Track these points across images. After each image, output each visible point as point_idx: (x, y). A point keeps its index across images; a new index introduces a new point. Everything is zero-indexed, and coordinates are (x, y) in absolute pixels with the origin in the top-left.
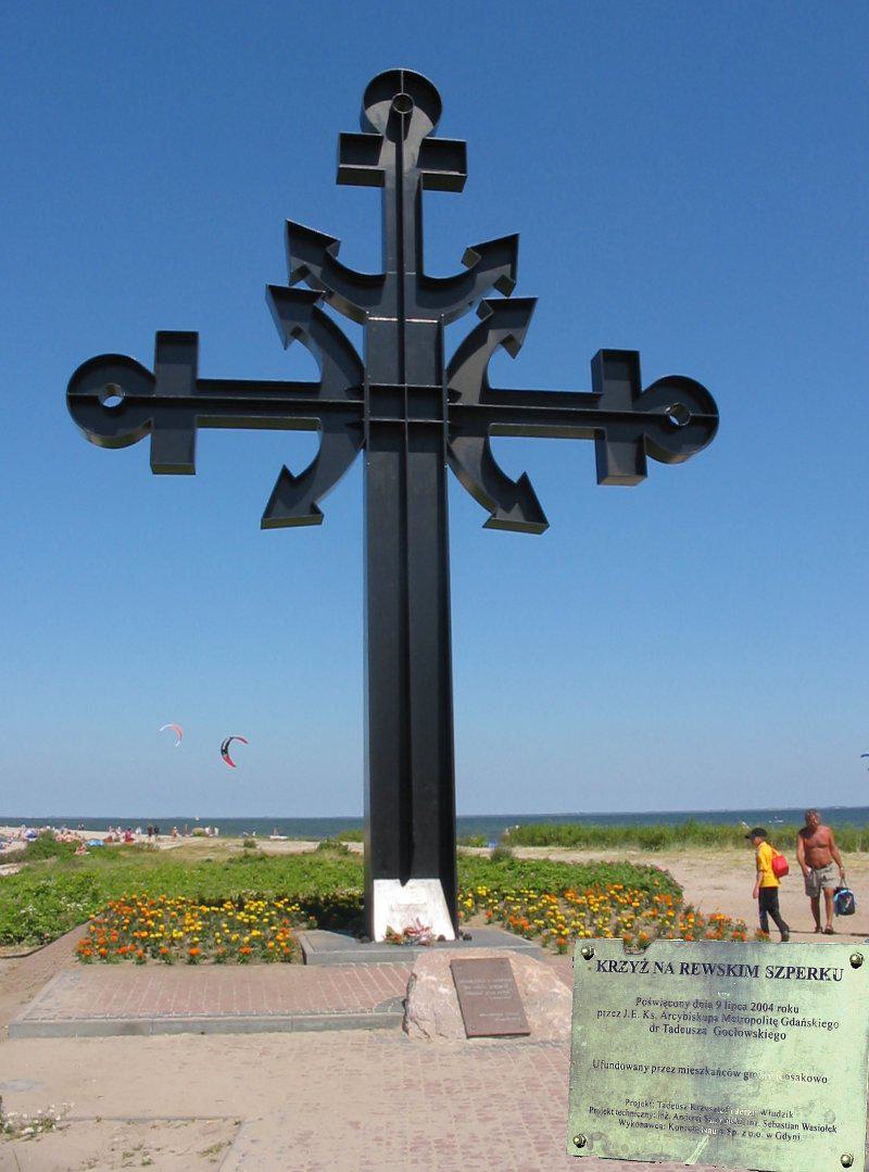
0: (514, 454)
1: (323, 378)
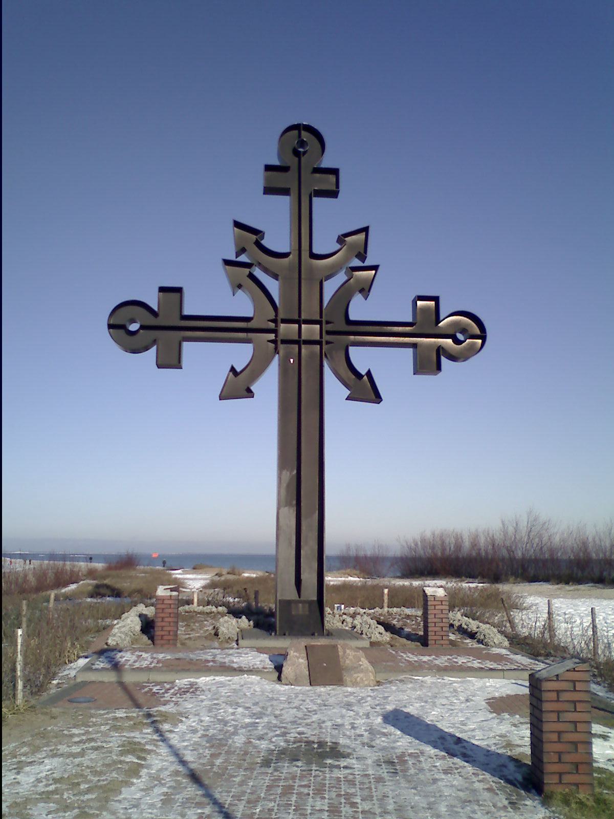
0: (362, 358)
1: (254, 315)
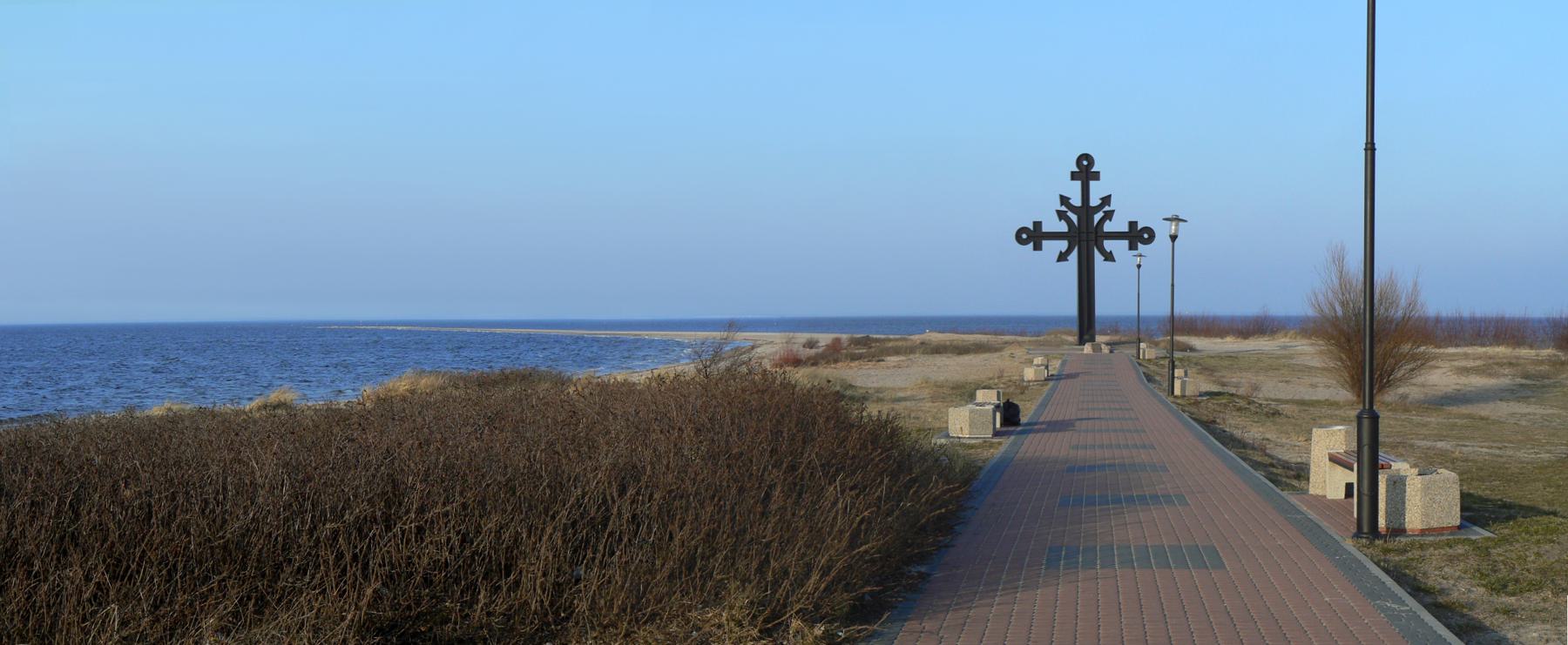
0: (1109, 245)
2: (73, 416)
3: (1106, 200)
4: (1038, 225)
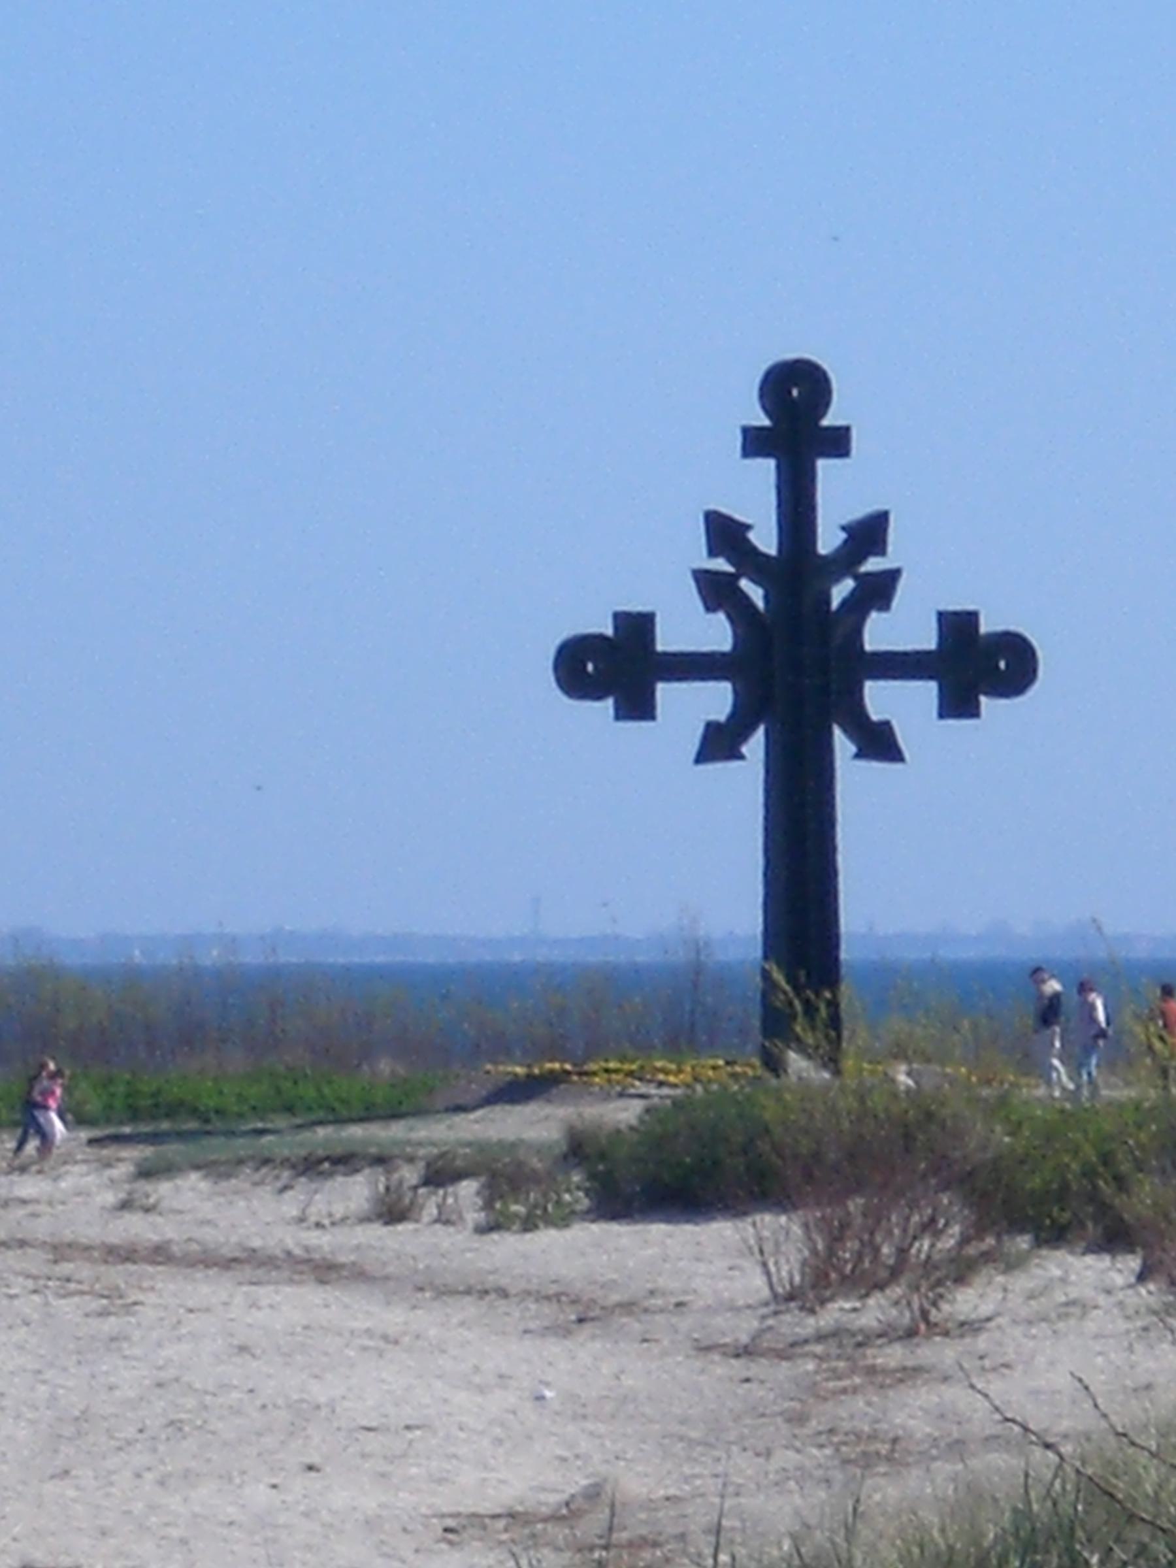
2: (495, 1139)
3: (869, 534)
4: (838, 443)
